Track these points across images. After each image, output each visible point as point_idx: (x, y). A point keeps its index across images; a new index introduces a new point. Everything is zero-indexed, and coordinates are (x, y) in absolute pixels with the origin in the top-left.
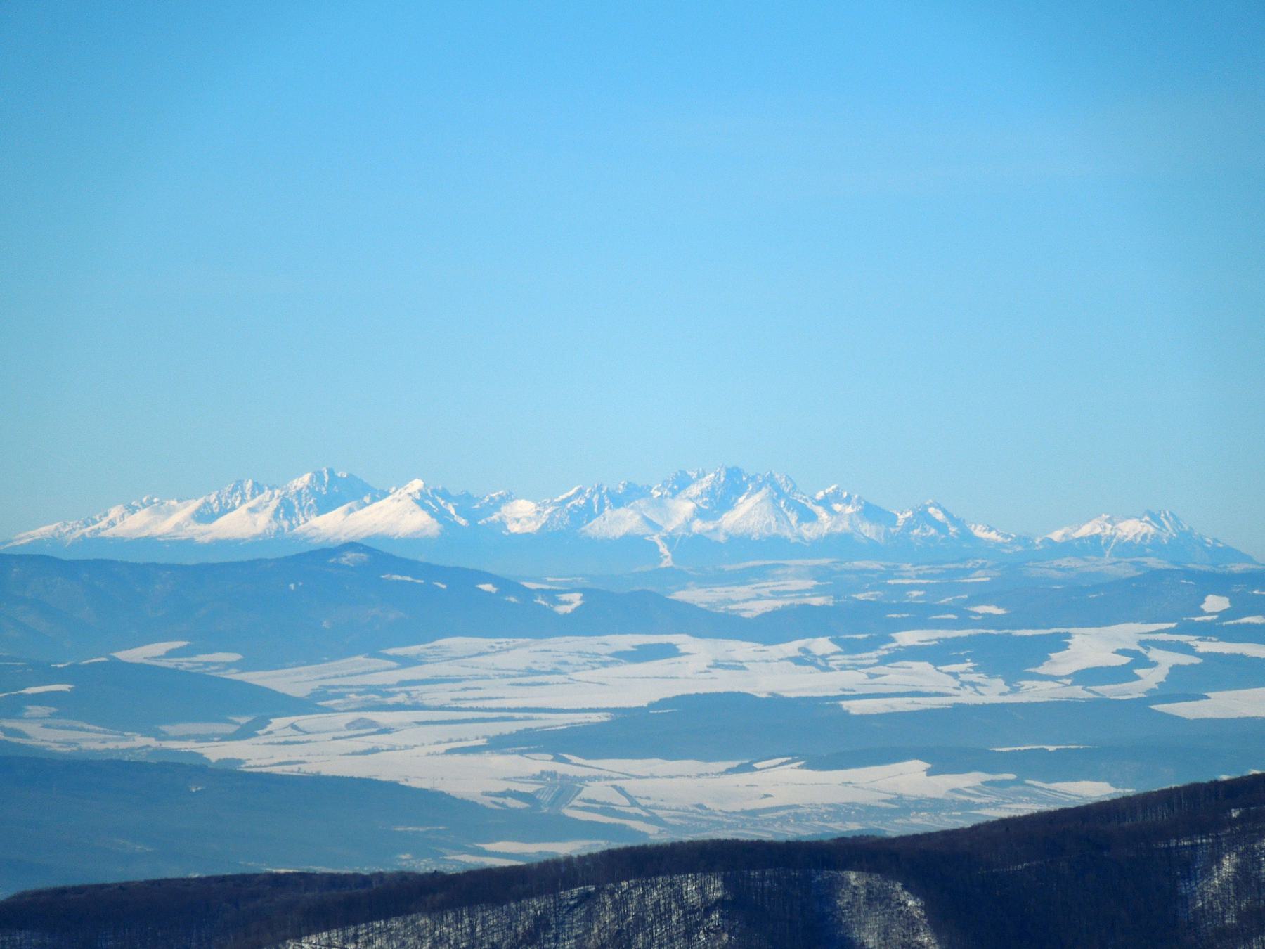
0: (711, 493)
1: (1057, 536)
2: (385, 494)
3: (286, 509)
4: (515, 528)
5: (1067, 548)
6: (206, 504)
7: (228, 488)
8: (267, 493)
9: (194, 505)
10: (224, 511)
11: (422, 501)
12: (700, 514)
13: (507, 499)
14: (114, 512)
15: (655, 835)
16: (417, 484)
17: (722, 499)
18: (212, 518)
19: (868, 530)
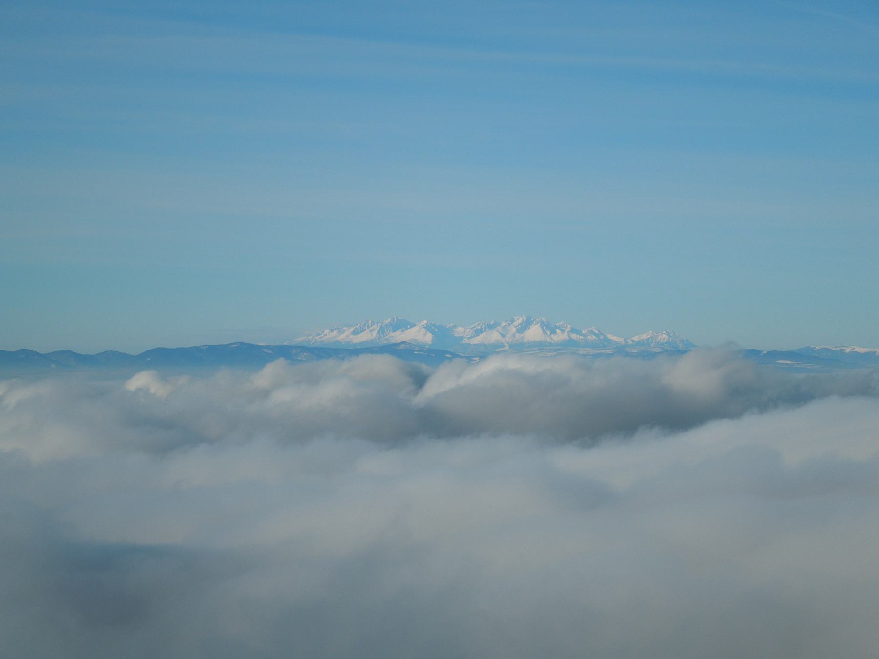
0: (521, 324)
1: (636, 339)
2: (413, 325)
3: (382, 330)
4: (456, 335)
5: (639, 343)
6: (356, 328)
7: (519, 321)
8: (375, 326)
9: (352, 329)
10: (362, 331)
11: (429, 328)
12: (518, 331)
13: (455, 326)
14: (326, 331)
15: (171, 344)
16: (425, 322)
17: (524, 327)
18: (358, 334)
19: (574, 336)
